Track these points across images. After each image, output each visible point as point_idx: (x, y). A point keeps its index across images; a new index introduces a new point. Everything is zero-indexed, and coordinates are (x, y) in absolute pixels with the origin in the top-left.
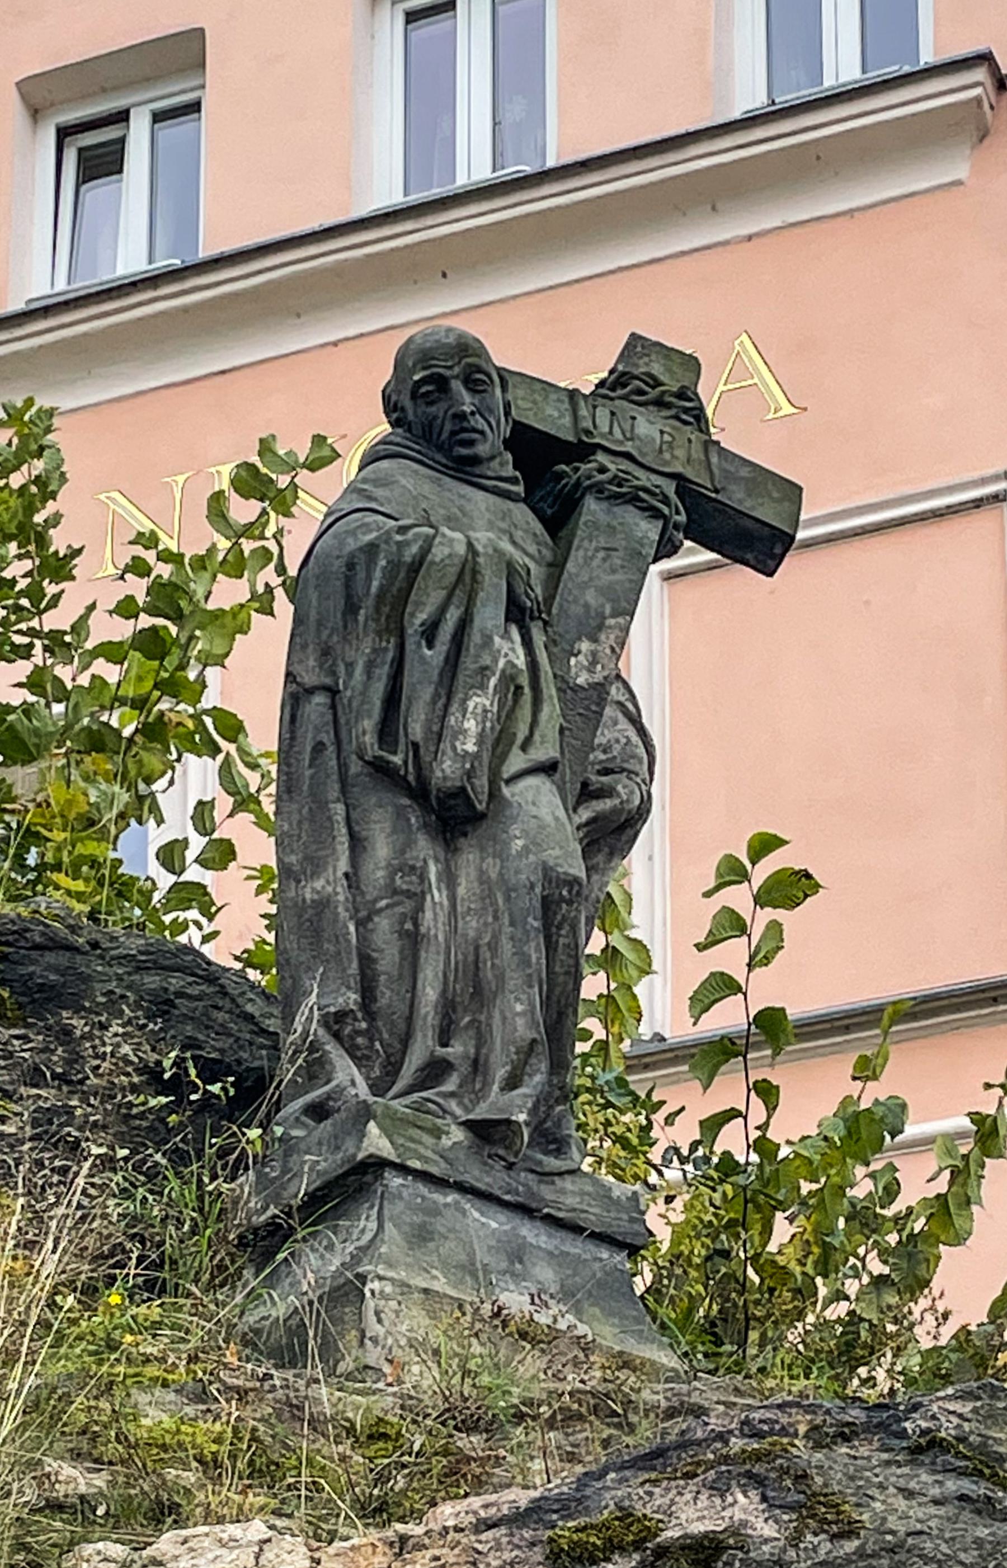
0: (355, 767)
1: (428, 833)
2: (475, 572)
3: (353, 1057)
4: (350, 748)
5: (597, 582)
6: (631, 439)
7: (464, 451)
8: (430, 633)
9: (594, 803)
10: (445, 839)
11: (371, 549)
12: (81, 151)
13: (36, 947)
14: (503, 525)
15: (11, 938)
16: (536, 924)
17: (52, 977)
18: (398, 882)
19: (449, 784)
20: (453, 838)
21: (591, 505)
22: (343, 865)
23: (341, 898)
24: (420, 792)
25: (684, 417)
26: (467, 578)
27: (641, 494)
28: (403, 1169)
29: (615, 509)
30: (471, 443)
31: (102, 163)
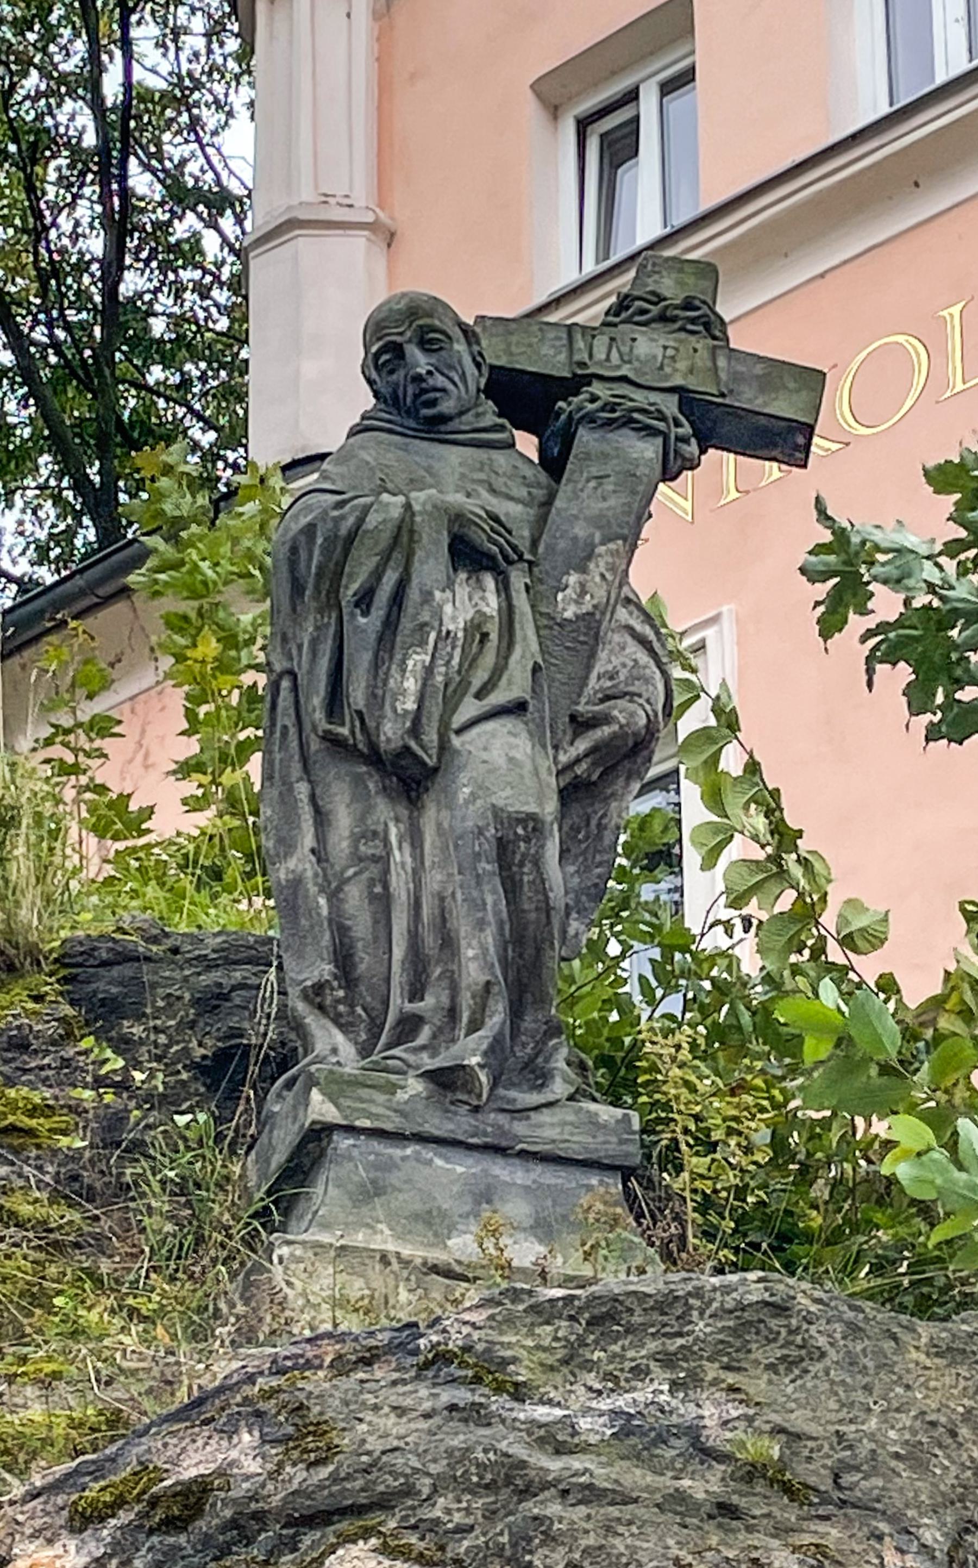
0: (315, 745)
1: (390, 797)
2: (412, 532)
3: (340, 1026)
4: (307, 727)
5: (587, 512)
6: (630, 362)
7: (426, 412)
8: (364, 600)
9: (590, 733)
10: (409, 798)
11: (310, 530)
12: (602, 136)
13: (104, 964)
14: (482, 476)
15: (80, 959)
16: (489, 867)
17: (114, 990)
18: (362, 848)
19: (393, 746)
20: (419, 797)
21: (585, 437)
22: (309, 841)
23: (309, 874)
24: (374, 757)
25: (690, 327)
26: (405, 539)
27: (636, 415)
28: (350, 1130)
29: (610, 435)
30: (433, 403)
31: (621, 148)
